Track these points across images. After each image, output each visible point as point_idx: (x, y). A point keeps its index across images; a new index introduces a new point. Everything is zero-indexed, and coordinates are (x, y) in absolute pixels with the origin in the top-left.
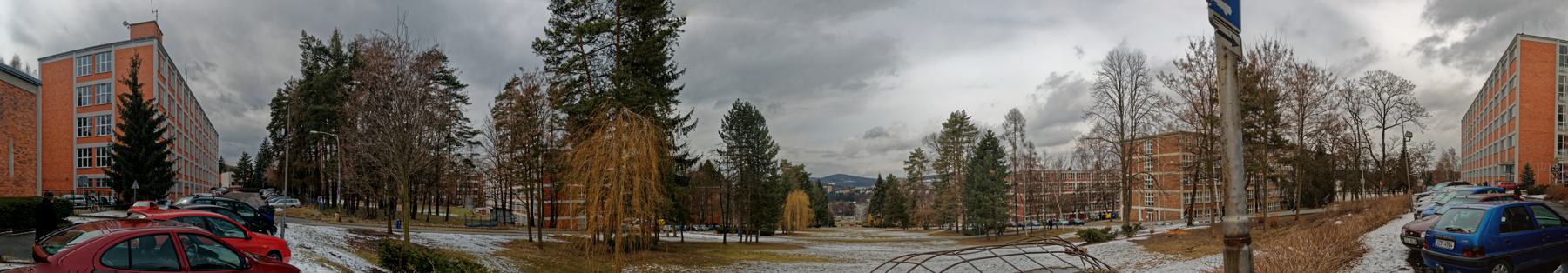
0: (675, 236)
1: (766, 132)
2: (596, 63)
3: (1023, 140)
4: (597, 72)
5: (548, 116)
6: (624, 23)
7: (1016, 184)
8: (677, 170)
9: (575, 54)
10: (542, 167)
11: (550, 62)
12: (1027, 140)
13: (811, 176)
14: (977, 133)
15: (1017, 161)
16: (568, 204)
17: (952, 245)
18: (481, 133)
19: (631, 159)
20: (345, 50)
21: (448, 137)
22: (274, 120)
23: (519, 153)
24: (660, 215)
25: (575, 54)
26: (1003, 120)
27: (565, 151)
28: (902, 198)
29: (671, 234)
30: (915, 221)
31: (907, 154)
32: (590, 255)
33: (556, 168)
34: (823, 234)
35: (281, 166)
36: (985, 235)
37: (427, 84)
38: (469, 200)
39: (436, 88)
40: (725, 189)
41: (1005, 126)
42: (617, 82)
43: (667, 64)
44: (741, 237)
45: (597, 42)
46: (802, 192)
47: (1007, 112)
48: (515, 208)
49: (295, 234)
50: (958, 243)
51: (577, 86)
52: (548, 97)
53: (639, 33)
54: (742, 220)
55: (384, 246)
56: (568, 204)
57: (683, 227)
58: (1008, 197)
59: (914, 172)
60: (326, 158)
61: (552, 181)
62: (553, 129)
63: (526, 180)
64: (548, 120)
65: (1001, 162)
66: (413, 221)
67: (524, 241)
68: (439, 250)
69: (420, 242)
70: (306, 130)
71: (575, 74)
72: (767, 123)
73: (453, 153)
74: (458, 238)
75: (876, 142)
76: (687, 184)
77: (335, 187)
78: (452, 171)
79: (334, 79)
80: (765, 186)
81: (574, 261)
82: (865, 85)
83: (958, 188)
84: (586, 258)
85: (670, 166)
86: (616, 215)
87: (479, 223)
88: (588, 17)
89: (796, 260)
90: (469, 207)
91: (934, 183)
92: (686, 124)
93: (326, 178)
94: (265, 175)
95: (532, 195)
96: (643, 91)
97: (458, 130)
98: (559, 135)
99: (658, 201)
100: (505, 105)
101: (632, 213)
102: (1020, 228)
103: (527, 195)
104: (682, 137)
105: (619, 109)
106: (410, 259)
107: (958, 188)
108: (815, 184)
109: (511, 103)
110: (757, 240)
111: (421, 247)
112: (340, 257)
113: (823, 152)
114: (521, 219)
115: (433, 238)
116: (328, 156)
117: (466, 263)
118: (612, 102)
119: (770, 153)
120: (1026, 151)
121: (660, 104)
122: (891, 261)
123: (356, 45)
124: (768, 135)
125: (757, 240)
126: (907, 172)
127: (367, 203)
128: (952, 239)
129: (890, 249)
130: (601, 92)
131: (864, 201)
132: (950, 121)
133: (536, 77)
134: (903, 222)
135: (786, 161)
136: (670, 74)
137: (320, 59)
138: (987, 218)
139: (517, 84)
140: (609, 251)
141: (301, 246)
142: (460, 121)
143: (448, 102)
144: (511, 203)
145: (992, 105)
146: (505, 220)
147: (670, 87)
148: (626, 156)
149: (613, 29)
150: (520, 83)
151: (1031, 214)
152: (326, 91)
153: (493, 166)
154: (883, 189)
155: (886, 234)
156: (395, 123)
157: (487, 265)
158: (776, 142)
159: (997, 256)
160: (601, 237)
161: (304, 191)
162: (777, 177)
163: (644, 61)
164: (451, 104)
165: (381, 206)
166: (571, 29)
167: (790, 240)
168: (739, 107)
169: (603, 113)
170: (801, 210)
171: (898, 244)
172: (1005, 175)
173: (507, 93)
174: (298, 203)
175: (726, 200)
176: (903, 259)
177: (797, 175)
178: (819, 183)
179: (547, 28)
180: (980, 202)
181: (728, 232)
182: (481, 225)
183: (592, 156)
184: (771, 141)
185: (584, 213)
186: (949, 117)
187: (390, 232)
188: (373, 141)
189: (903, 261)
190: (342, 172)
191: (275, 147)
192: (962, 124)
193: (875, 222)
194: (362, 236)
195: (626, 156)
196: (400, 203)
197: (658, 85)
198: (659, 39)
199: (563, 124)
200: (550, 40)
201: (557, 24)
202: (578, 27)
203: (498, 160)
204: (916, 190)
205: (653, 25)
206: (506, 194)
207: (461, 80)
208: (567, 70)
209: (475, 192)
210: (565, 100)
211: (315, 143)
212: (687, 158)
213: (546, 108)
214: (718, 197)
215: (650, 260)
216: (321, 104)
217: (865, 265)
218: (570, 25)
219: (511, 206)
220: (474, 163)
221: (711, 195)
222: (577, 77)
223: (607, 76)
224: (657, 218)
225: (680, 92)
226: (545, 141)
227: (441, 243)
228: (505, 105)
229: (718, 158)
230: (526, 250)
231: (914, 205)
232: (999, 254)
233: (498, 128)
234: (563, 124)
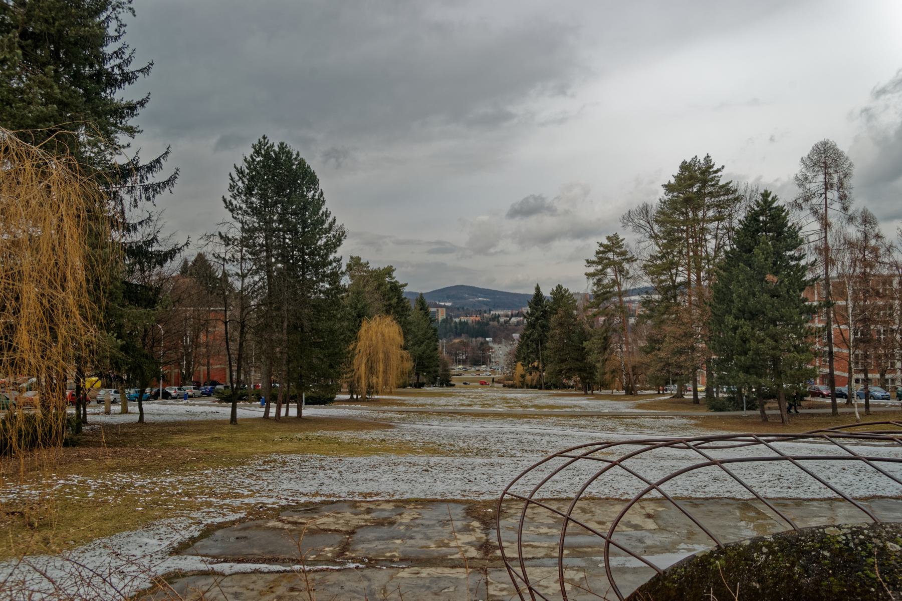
0: (125, 411)
1: (318, 203)
3: (845, 209)
7: (829, 304)
12: (857, 205)
13: (406, 290)
14: (737, 199)
15: (832, 255)
17: (685, 428)
26: (796, 168)
28: (583, 332)
30: (607, 376)
31: (592, 246)
34: (429, 400)
36: (758, 412)
41: (802, 181)
43: (109, 49)
44: (268, 408)
46: (388, 320)
47: (806, 150)
50: (696, 425)
54: (269, 374)
57: (142, 392)
58: (810, 332)
59: (606, 282)
65: (792, 258)
72: (322, 185)
75: (532, 223)
76: (151, 303)
80: (317, 307)
82: (508, 116)
83: (696, 312)
89: (376, 451)
91: (645, 303)
92: (153, 179)
102: (839, 401)
107: (696, 312)
108: (413, 305)
110: (299, 412)
119: (326, 244)
120: (854, 232)
121: (90, 131)
122: (560, 454)
124: (323, 209)
126: (592, 281)
128: (683, 417)
129: (557, 430)
131: (509, 338)
132: (678, 178)
134: (583, 380)
136: (116, 71)
138: (760, 376)
145: (772, 139)
151: (865, 372)
154: (545, 315)
158: (338, 223)
159: (784, 458)
162: (340, 290)
163: (53, 31)
167: (366, 413)
171: (573, 421)
172: (803, 286)
175: (237, 334)
176: (583, 451)
177: (380, 285)
178: (421, 302)
180: (745, 341)
181: (240, 399)
184: (330, 220)
186: (677, 171)
189: (584, 456)
192: (704, 183)
193: (528, 377)
197: (85, 90)
204: (610, 316)
212: (155, 248)
214: (221, 328)
217: (509, 461)
224: (80, 373)
225: (139, 110)
229: (221, 250)
231: (605, 346)
232: (789, 453)
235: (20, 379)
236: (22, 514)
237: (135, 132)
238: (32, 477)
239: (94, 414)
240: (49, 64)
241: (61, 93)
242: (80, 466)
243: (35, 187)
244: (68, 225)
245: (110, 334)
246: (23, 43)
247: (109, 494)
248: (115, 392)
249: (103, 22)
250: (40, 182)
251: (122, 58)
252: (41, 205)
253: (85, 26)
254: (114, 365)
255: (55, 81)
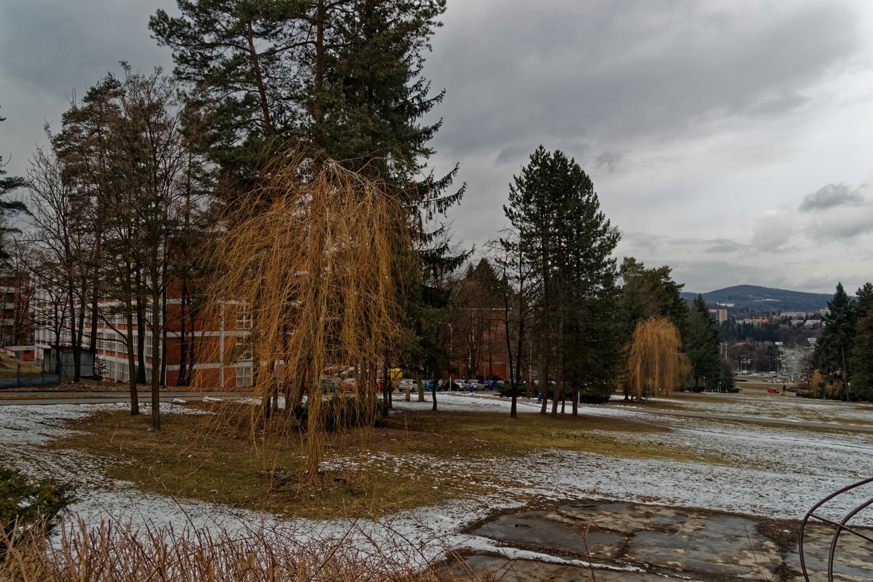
0: (422, 400)
2: (278, 73)
4: (279, 90)
8: (426, 276)
13: (683, 290)
16: (217, 338)
19: (341, 255)
23: (114, 234)
29: (414, 396)
32: (257, 436)
34: (710, 406)
40: (514, 312)
42: (317, 112)
43: (410, 83)
46: (664, 321)
53: (359, 25)
54: (546, 371)
56: (217, 338)
57: (436, 383)
61: (185, 292)
62: (189, 191)
67: (121, 413)
71: (237, 89)
72: (596, 189)
76: (443, 304)
80: (592, 308)
81: (224, 450)
82: (801, 101)
84: (250, 444)
85: (414, 270)
86: (310, 360)
87: (15, 381)
95: (141, 320)
96: (365, 131)
98: (203, 204)
99: (391, 334)
100: (85, 133)
101: (340, 357)
104: (437, 216)
105: (319, 162)
108: (690, 306)
110: (575, 410)
113: (709, 242)
114: (116, 370)
118: (306, 148)
119: (600, 246)
121: (396, 156)
124: (598, 212)
130: (287, 128)
131: (803, 342)
133: (156, 86)
135: (633, 260)
136: (416, 102)
139: (115, 95)
140: (295, 429)
144: (94, 336)
147: (415, 125)
148: (331, 249)
149: (311, 13)
150: (121, 94)
155: (859, 415)
158: (612, 225)
160: (282, 402)
163: (368, 75)
167: (641, 415)
168: (544, 161)
169: (289, 168)
170: (663, 357)
173: (91, 107)
178: (700, 302)
182: (19, 385)
185: (248, 356)
193: (828, 387)
195: (331, 249)
197: (392, 121)
198: (397, 38)
200: (188, 19)
203: (67, 245)
205: (385, 12)
206: (82, 317)
208: (221, 79)
210: (215, 138)
212: (446, 255)
213: (176, 150)
214: (502, 328)
215: (374, 445)
217: (809, 479)
219: (93, 344)
221: (489, 324)
222: (240, 96)
223: (297, 98)
224: (388, 365)
225: (434, 134)
226: (172, 213)
228: (85, 133)
229: (503, 255)
233: (67, 177)
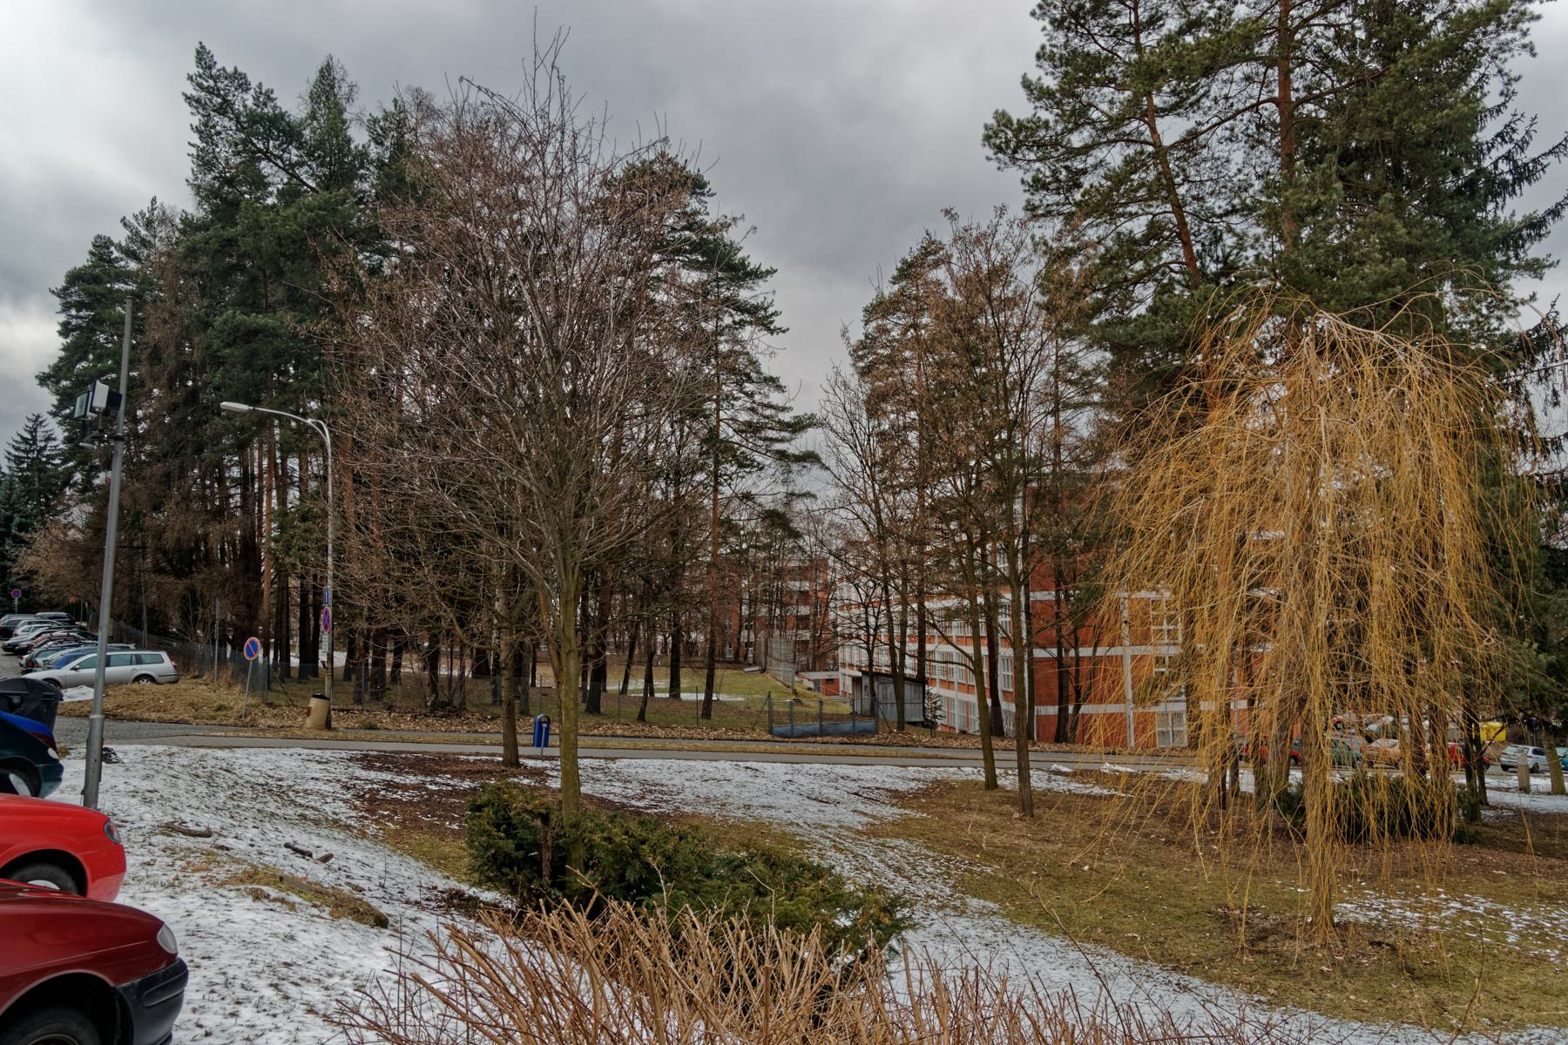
4: (1210, 202)
5: (1041, 363)
6: (1305, 22)
9: (1131, 151)
10: (1026, 534)
11: (1045, 187)
18: (821, 424)
20: (359, 137)
21: (712, 438)
22: (74, 353)
23: (947, 488)
24: (1485, 710)
25: (1131, 151)
27: (1103, 477)
29: (1541, 783)
32: (1206, 843)
33: (1075, 534)
35: (97, 527)
37: (640, 266)
38: (780, 647)
39: (671, 280)
42: (1286, 227)
43: (1488, 131)
45: (1206, 103)
48: (936, 672)
49: (146, 785)
51: (1141, 256)
52: (1039, 297)
55: (488, 812)
60: (283, 501)
61: (1060, 580)
62: (1058, 405)
63: (973, 578)
64: (1042, 376)
66: (592, 720)
68: (680, 817)
69: (615, 791)
70: (204, 398)
71: (1132, 216)
73: (726, 491)
74: (743, 776)
77: (311, 605)
78: (722, 551)
79: (315, 228)
81: (1147, 862)
87: (815, 726)
88: (1172, 25)
90: (781, 672)
93: (282, 573)
94: (28, 561)
96: (1392, 249)
97: (744, 417)
98: (1083, 424)
100: (895, 333)
103: (975, 627)
106: (580, 853)
109: (915, 326)
111: (619, 810)
112: (326, 859)
114: (957, 711)
115: (662, 777)
116: (294, 494)
117: (772, 863)
123: (401, 124)
125: (1077, 653)
127: (432, 662)
130: (1228, 267)
136: (1504, 166)
137: (267, 156)
139: (936, 264)
141: (170, 829)
142: (749, 387)
143: (709, 326)
144: (921, 655)
146: (901, 712)
149: (1264, 48)
150: (947, 260)
152: (287, 266)
153: (861, 534)
156: (532, 389)
157: (843, 867)
160: (1247, 781)
161: (189, 620)
163: (1389, 135)
164: (718, 332)
165: (481, 671)
166: (1116, 71)
173: (902, 291)
174: (164, 665)
179: (1033, 77)
182: (823, 732)
183: (1205, 491)
187: (512, 761)
188: (455, 448)
190: (339, 551)
191: (74, 449)
194: (411, 779)
195: (1332, 485)
196: (548, 661)
198: (1451, 48)
199: (1093, 388)
200: (1044, 115)
201: (1064, 61)
202: (1139, 62)
203: (877, 512)
206: (904, 625)
207: (753, 254)
208: (1104, 206)
209: (802, 621)
210: (1099, 308)
211: (241, 447)
213: (1034, 337)
216: (270, 309)
218: (1111, 58)
219: (921, 668)
220: (798, 524)
222: (1138, 227)
223: (1246, 210)
224: (1471, 719)
225: (1553, 226)
227: (688, 795)
230: (975, 817)
234: (1093, 388)
235: (1366, 717)
236: (1393, 948)
237: (1545, 267)
238: (1403, 887)
239: (1499, 789)
240: (1385, 190)
241: (1409, 233)
242: (1486, 882)
243: (1379, 398)
244: (1439, 450)
245: (1526, 644)
246: (1344, 170)
247: (1547, 944)
248: (1535, 752)
249: (1474, 89)
250: (1388, 389)
251: (1512, 140)
252: (1392, 426)
253: (1442, 108)
254: (1536, 702)
255: (1397, 216)
